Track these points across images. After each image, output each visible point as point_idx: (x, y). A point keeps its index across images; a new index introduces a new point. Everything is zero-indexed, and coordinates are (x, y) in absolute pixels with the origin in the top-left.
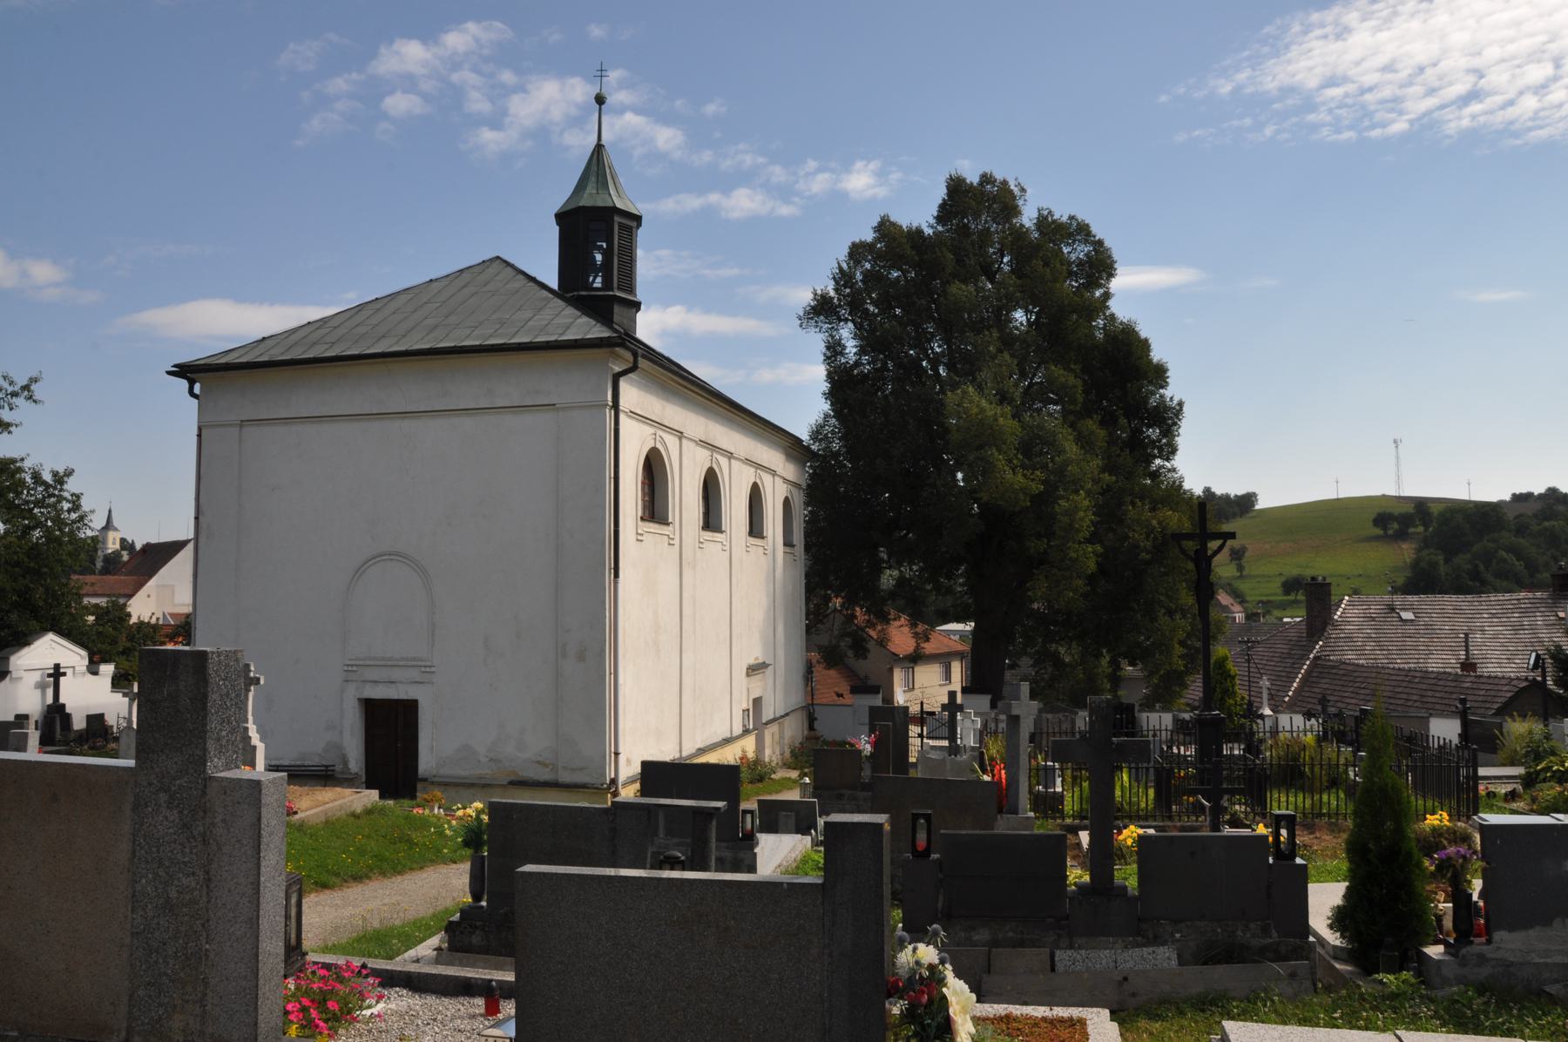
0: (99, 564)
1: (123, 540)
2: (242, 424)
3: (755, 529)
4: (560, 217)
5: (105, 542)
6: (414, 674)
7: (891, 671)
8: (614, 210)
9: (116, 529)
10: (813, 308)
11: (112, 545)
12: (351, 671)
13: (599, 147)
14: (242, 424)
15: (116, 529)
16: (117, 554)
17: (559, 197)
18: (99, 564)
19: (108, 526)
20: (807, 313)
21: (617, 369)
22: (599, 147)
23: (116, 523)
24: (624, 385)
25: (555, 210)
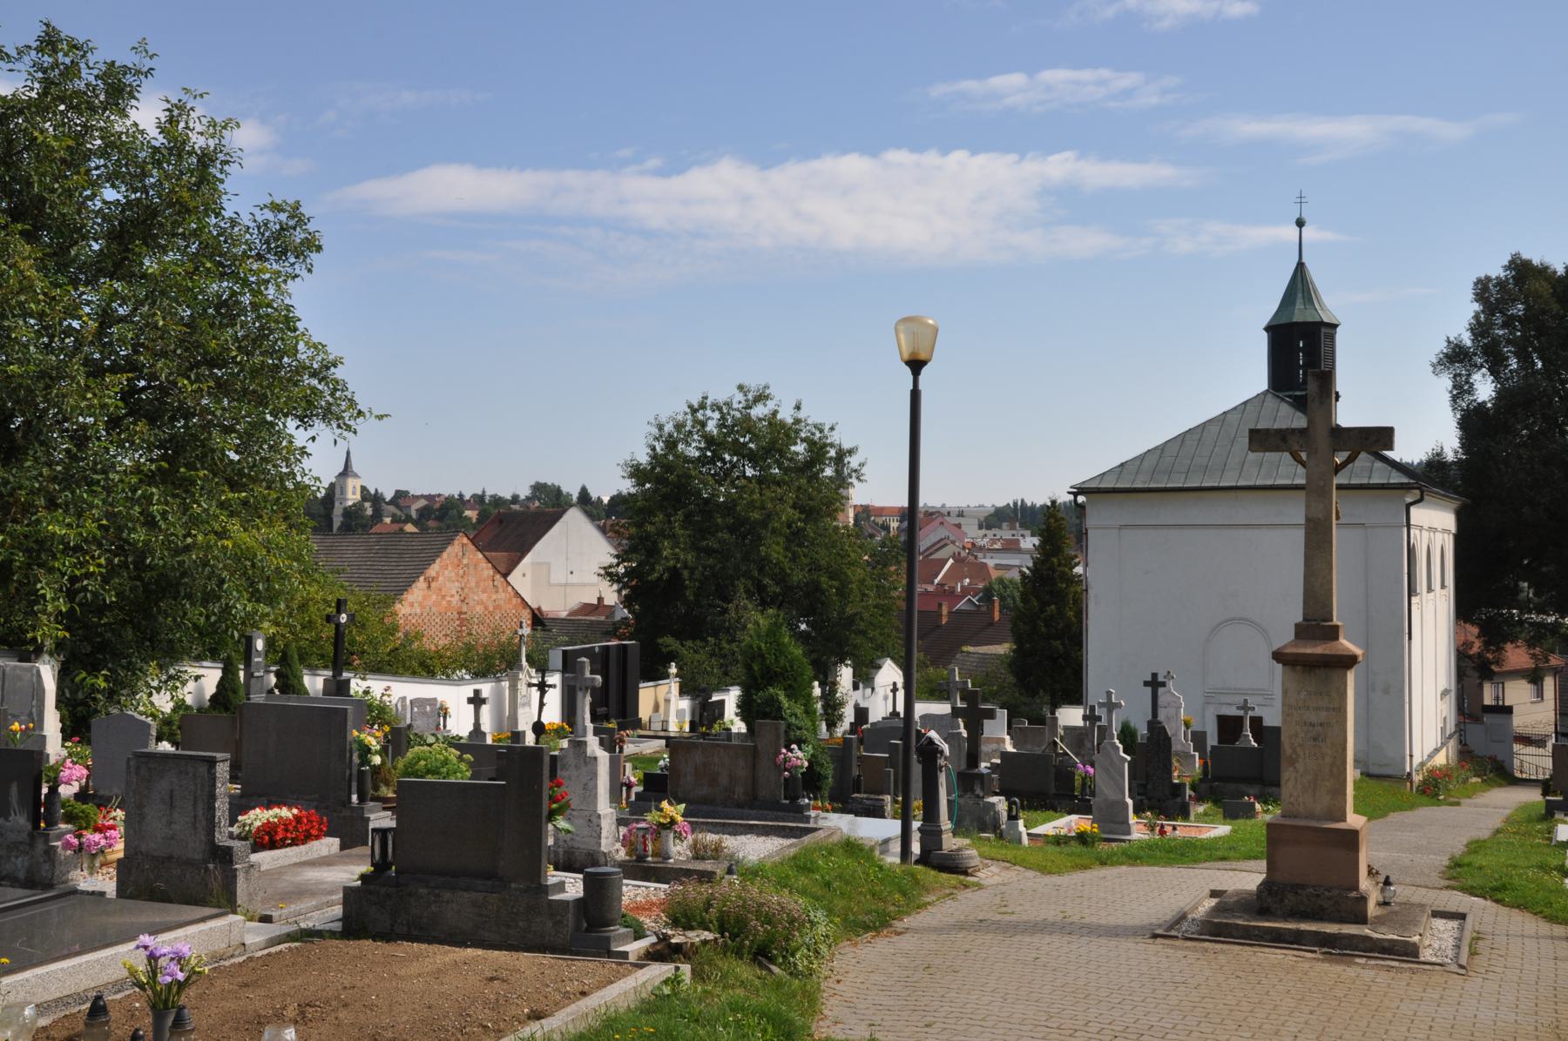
0: (337, 521)
1: (363, 489)
2: (1122, 527)
3: (1443, 586)
4: (1268, 329)
5: (343, 491)
6: (1259, 700)
7: (1481, 687)
8: (1322, 324)
9: (356, 476)
10: (1446, 355)
11: (352, 497)
12: (1209, 698)
13: (1300, 266)
14: (1122, 527)
15: (356, 476)
16: (358, 507)
17: (1268, 308)
18: (337, 521)
19: (347, 472)
20: (1440, 362)
21: (1409, 500)
22: (1300, 266)
23: (355, 467)
24: (1413, 510)
25: (1265, 321)
